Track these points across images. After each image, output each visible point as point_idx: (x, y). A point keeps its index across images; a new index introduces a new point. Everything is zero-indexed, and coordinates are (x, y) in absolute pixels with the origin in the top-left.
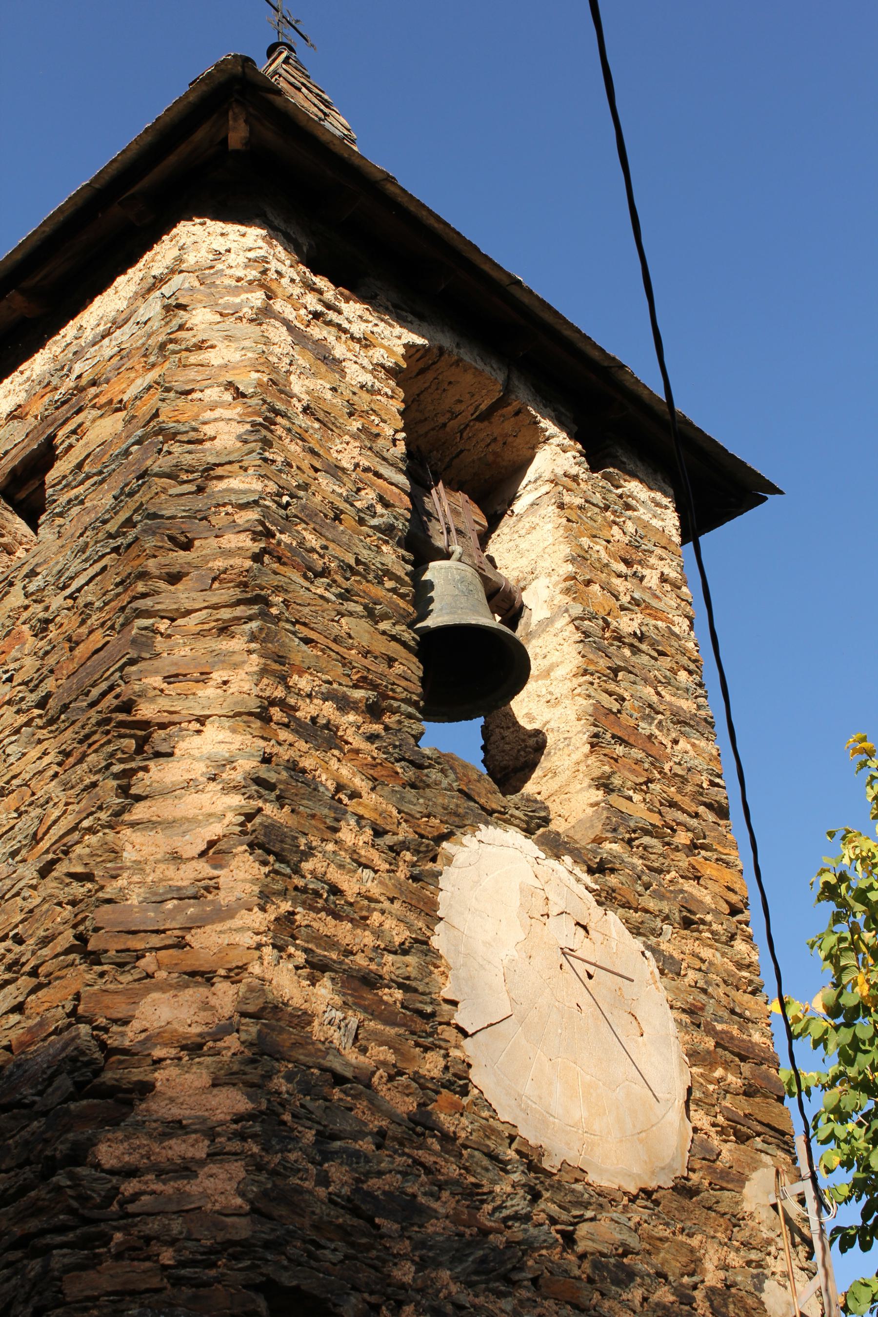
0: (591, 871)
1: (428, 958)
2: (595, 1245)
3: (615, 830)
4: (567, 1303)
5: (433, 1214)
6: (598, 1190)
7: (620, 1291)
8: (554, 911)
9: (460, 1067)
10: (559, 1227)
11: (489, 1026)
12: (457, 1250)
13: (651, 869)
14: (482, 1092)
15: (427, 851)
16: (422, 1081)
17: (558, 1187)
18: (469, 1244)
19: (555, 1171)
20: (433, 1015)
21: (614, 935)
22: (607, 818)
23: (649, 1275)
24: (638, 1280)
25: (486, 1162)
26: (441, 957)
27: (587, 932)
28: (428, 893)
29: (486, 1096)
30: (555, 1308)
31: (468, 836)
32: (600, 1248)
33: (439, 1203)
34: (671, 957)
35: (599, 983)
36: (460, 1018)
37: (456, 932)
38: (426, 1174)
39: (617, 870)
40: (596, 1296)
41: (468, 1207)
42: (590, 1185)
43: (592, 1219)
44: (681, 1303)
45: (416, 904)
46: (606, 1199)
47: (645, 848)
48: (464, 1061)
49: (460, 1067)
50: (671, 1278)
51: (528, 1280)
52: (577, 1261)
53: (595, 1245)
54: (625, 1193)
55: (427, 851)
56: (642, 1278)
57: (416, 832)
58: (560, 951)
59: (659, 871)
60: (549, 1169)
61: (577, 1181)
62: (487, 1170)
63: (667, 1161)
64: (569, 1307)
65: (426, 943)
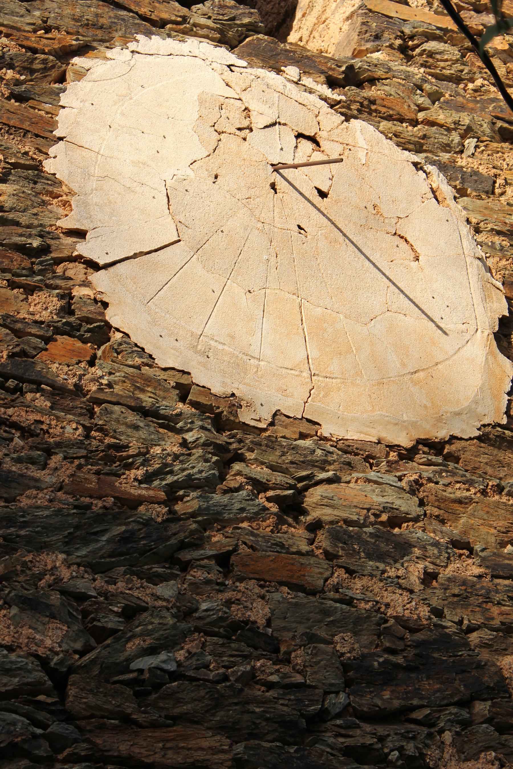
0: (332, 83)
1: (39, 186)
2: (336, 512)
3: (377, 37)
4: (282, 583)
5: (37, 484)
6: (340, 444)
7: (382, 566)
8: (258, 122)
9: (92, 308)
10: (270, 493)
11: (135, 256)
12: (77, 527)
13: (439, 78)
14: (128, 335)
15: (45, 69)
16: (19, 326)
17: (272, 443)
18: (99, 518)
19: (263, 425)
20: (45, 250)
21: (361, 142)
22: (363, 23)
23: (436, 544)
24: (417, 552)
25: (132, 417)
26: (60, 183)
27: (318, 144)
28: (42, 113)
29: (134, 339)
30: (257, 590)
31: (117, 49)
32: (344, 515)
33: (46, 471)
34: (476, 173)
35: (337, 202)
36: (83, 249)
37: (85, 153)
38: (22, 437)
39: (379, 79)
40: (340, 574)
41: (98, 473)
42: (325, 439)
43: (329, 481)
44: (494, 577)
45: (17, 124)
46: (356, 456)
47: (431, 54)
48: (95, 301)
49: (92, 308)
50: (478, 547)
51: (209, 558)
52: (307, 535)
53: (336, 512)
54: (391, 447)
55: (45, 70)
56: (424, 548)
57: (22, 46)
58: (270, 169)
59: (457, 80)
60: (253, 423)
61: (303, 436)
62: (136, 428)
63: (466, 404)
64: (286, 589)
65: (38, 167)
